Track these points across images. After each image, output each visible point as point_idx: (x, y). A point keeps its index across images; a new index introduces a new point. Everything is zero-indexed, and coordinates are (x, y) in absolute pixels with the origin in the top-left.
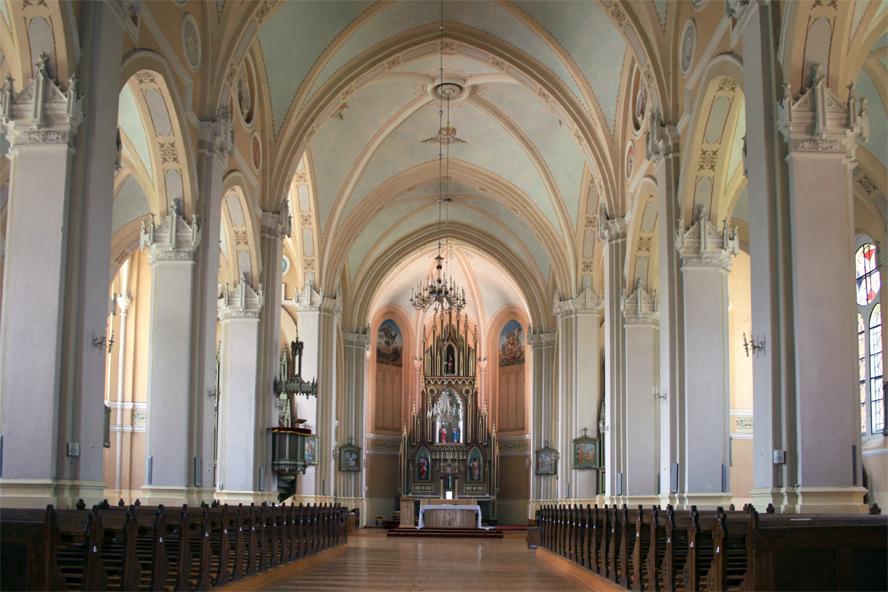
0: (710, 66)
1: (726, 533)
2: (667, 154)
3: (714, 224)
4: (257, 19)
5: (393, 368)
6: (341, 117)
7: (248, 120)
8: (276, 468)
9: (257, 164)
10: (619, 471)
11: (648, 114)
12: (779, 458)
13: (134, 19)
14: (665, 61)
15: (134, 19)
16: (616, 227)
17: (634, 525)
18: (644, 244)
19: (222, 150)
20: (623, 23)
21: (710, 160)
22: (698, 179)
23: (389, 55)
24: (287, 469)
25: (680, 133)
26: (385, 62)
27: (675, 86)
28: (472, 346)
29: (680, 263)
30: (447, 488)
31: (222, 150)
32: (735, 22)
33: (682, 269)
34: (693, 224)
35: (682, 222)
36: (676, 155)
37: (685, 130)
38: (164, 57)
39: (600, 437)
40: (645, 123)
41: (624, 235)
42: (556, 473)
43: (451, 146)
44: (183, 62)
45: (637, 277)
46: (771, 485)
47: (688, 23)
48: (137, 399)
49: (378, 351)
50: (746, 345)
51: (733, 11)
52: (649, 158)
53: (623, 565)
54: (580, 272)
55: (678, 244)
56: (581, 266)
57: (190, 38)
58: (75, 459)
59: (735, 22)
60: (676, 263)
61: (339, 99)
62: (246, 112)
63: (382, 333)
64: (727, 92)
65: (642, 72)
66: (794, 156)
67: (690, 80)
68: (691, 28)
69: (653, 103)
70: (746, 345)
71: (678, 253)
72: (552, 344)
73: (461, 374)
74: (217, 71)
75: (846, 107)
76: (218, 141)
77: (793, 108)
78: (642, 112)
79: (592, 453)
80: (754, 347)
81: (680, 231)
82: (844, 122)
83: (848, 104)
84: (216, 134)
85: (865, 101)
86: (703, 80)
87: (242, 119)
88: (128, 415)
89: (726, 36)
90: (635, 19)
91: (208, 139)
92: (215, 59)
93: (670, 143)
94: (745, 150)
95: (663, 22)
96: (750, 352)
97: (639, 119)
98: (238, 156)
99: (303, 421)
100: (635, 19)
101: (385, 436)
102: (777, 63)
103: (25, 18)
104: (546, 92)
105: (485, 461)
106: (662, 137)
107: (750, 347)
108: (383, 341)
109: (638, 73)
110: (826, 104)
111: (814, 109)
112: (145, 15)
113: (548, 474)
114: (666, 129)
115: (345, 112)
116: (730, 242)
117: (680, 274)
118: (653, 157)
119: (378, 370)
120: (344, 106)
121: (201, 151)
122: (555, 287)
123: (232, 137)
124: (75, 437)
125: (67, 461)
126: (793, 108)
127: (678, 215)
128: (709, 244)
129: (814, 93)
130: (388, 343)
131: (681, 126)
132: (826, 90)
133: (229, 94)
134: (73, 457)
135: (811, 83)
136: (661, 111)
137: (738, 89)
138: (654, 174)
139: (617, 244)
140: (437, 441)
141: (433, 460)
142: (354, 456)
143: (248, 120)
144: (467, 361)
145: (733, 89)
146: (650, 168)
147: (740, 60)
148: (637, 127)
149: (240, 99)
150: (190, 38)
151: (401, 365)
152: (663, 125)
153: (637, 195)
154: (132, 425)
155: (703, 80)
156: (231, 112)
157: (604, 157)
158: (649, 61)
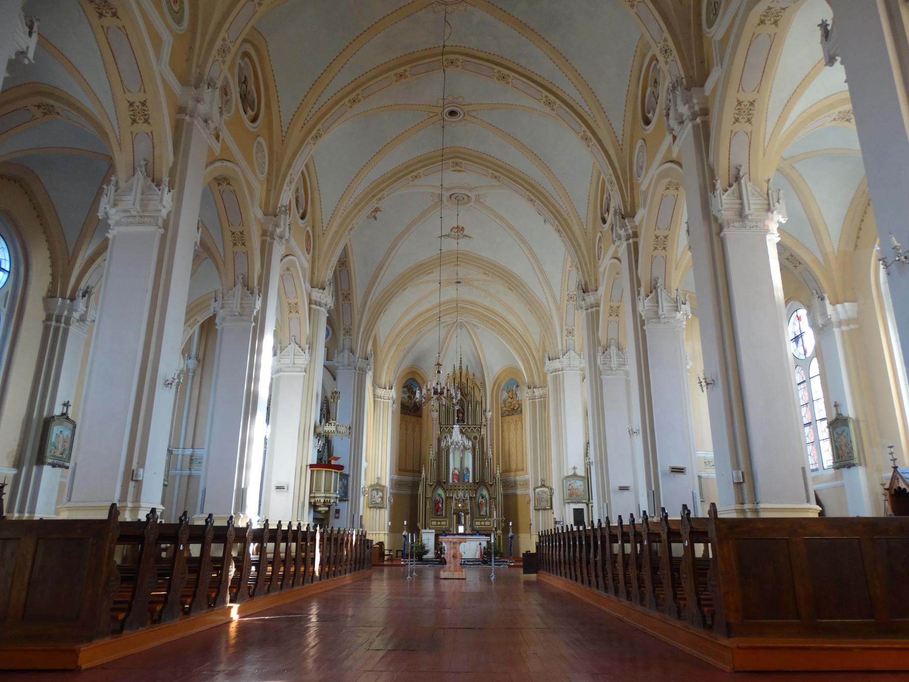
0: (658, 171)
1: (691, 527)
2: (628, 239)
3: (669, 292)
4: (312, 142)
5: (414, 419)
6: (375, 218)
7: (303, 218)
8: (312, 501)
9: (308, 251)
10: (604, 501)
11: (612, 210)
12: (738, 477)
13: (217, 137)
14: (624, 173)
15: (217, 137)
16: (591, 298)
17: (616, 536)
18: (615, 311)
19: (281, 238)
20: (591, 144)
21: (662, 243)
22: (653, 258)
23: (412, 171)
24: (322, 500)
25: (637, 223)
26: (409, 176)
27: (632, 189)
28: (479, 399)
29: (643, 323)
30: (459, 523)
31: (281, 238)
32: (675, 138)
33: (645, 328)
34: (651, 292)
35: (642, 290)
36: (635, 240)
37: (642, 220)
38: (237, 165)
39: (587, 479)
40: (610, 218)
41: (598, 305)
42: (551, 508)
43: (460, 241)
44: (254, 172)
45: (609, 337)
46: (734, 502)
47: (640, 142)
48: (196, 446)
49: (402, 404)
50: (700, 383)
51: (673, 130)
52: (614, 242)
53: (610, 575)
54: (565, 338)
55: (640, 308)
56: (565, 333)
57: (260, 155)
58: (139, 483)
59: (675, 138)
60: (640, 324)
61: (374, 204)
62: (301, 211)
63: (406, 390)
64: (672, 191)
65: (606, 180)
66: (728, 232)
67: (645, 182)
68: (642, 146)
69: (616, 202)
70: (700, 383)
71: (641, 316)
72: (544, 397)
73: (470, 423)
74: (280, 180)
75: (766, 196)
76: (278, 230)
77: (723, 197)
78: (608, 210)
79: (581, 489)
80: (708, 384)
81: (641, 297)
82: (766, 207)
83: (768, 194)
84: (277, 225)
85: (781, 191)
86: (653, 183)
87: (298, 216)
88: (187, 459)
89: (669, 150)
90: (599, 141)
91: (271, 229)
92: (278, 171)
93: (630, 231)
94: (688, 231)
95: (620, 142)
96: (705, 388)
97: (606, 216)
98: (293, 242)
99: (337, 459)
100: (599, 141)
101: (408, 478)
102: (709, 166)
103: (102, 27)
104: (533, 197)
105: (490, 498)
106: (623, 226)
107: (704, 384)
108: (406, 396)
109: (604, 182)
110: (750, 194)
111: (741, 197)
112: (225, 134)
113: (545, 509)
114: (626, 221)
115: (378, 215)
116: (683, 306)
117: (643, 331)
118: (617, 243)
119: (402, 420)
120: (377, 210)
121: (265, 238)
122: (544, 350)
123: (290, 228)
124: (142, 464)
125: (132, 484)
126: (723, 197)
127: (639, 286)
128: (665, 306)
129: (739, 185)
130: (409, 397)
131: (637, 218)
132: (748, 183)
133: (287, 196)
134: (136, 481)
135: (737, 179)
136: (622, 208)
137: (681, 189)
138: (619, 255)
139: (592, 313)
140: (451, 481)
141: (447, 498)
142: (380, 494)
143: (303, 218)
144: (475, 410)
145: (677, 189)
146: (616, 251)
147: (680, 165)
148: (604, 222)
149: (297, 201)
150: (260, 155)
151: (420, 416)
152: (623, 218)
153: (606, 273)
154: (190, 469)
155: (653, 183)
156: (290, 210)
157: (579, 246)
158: (611, 171)
